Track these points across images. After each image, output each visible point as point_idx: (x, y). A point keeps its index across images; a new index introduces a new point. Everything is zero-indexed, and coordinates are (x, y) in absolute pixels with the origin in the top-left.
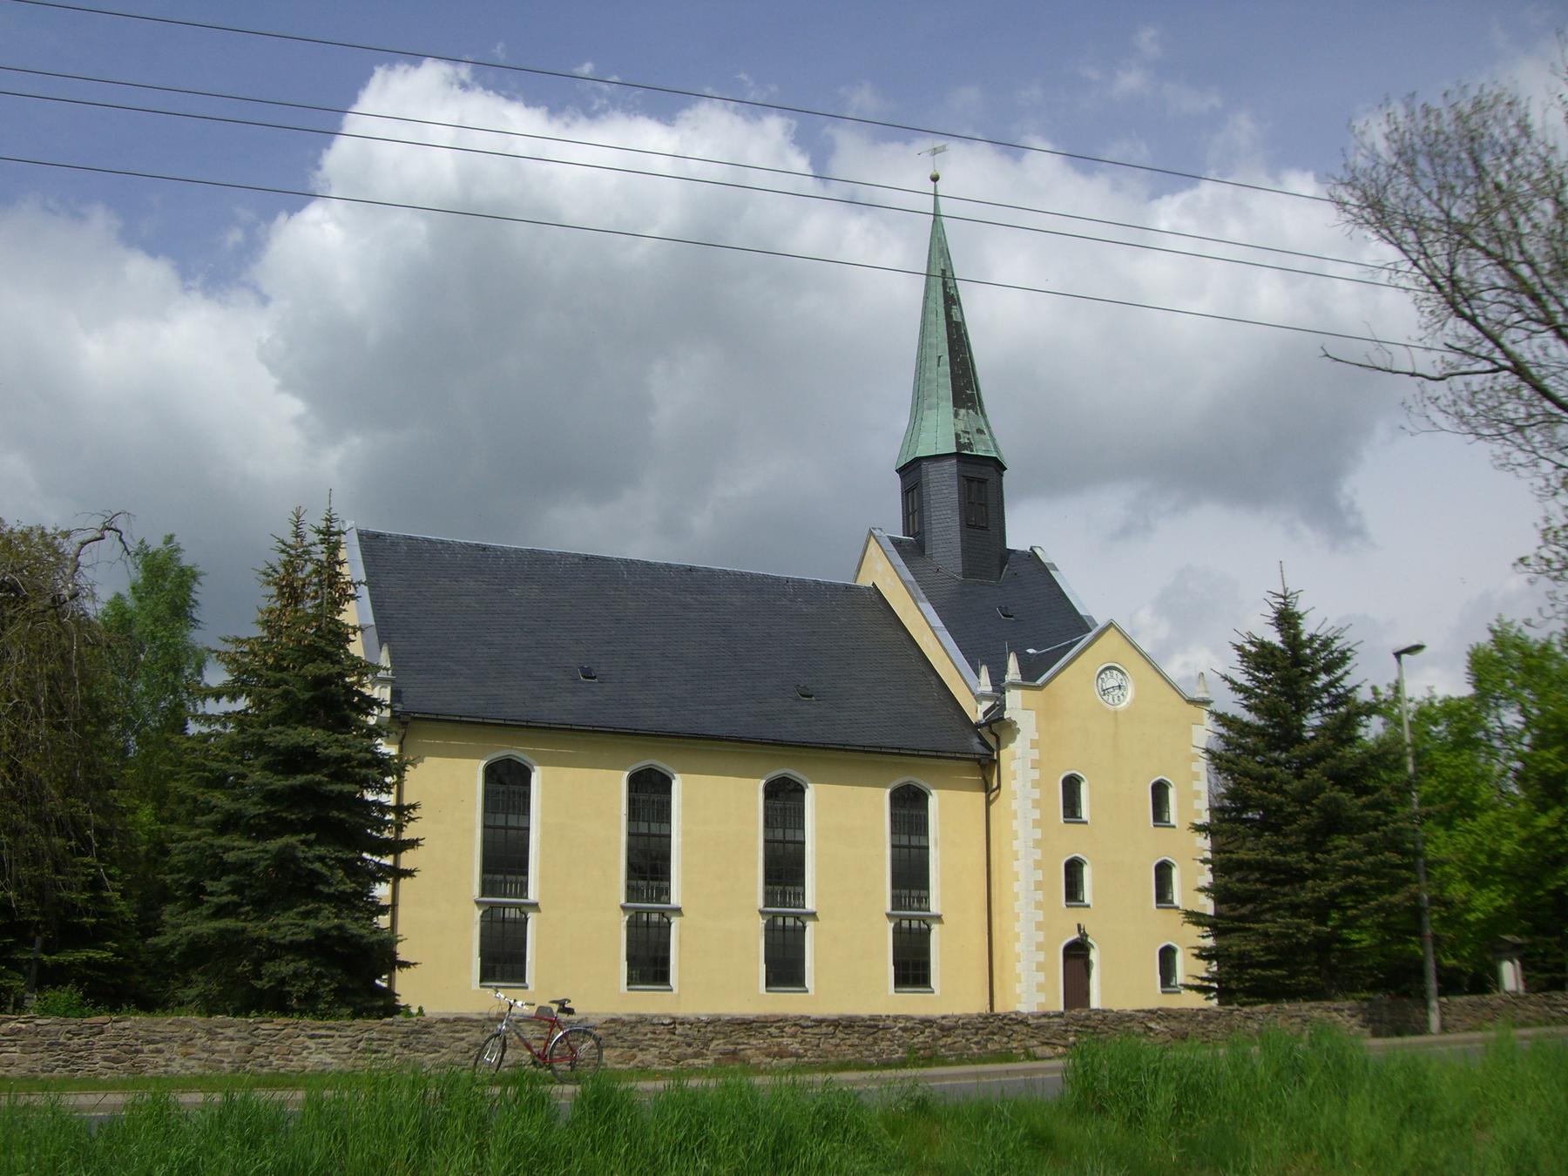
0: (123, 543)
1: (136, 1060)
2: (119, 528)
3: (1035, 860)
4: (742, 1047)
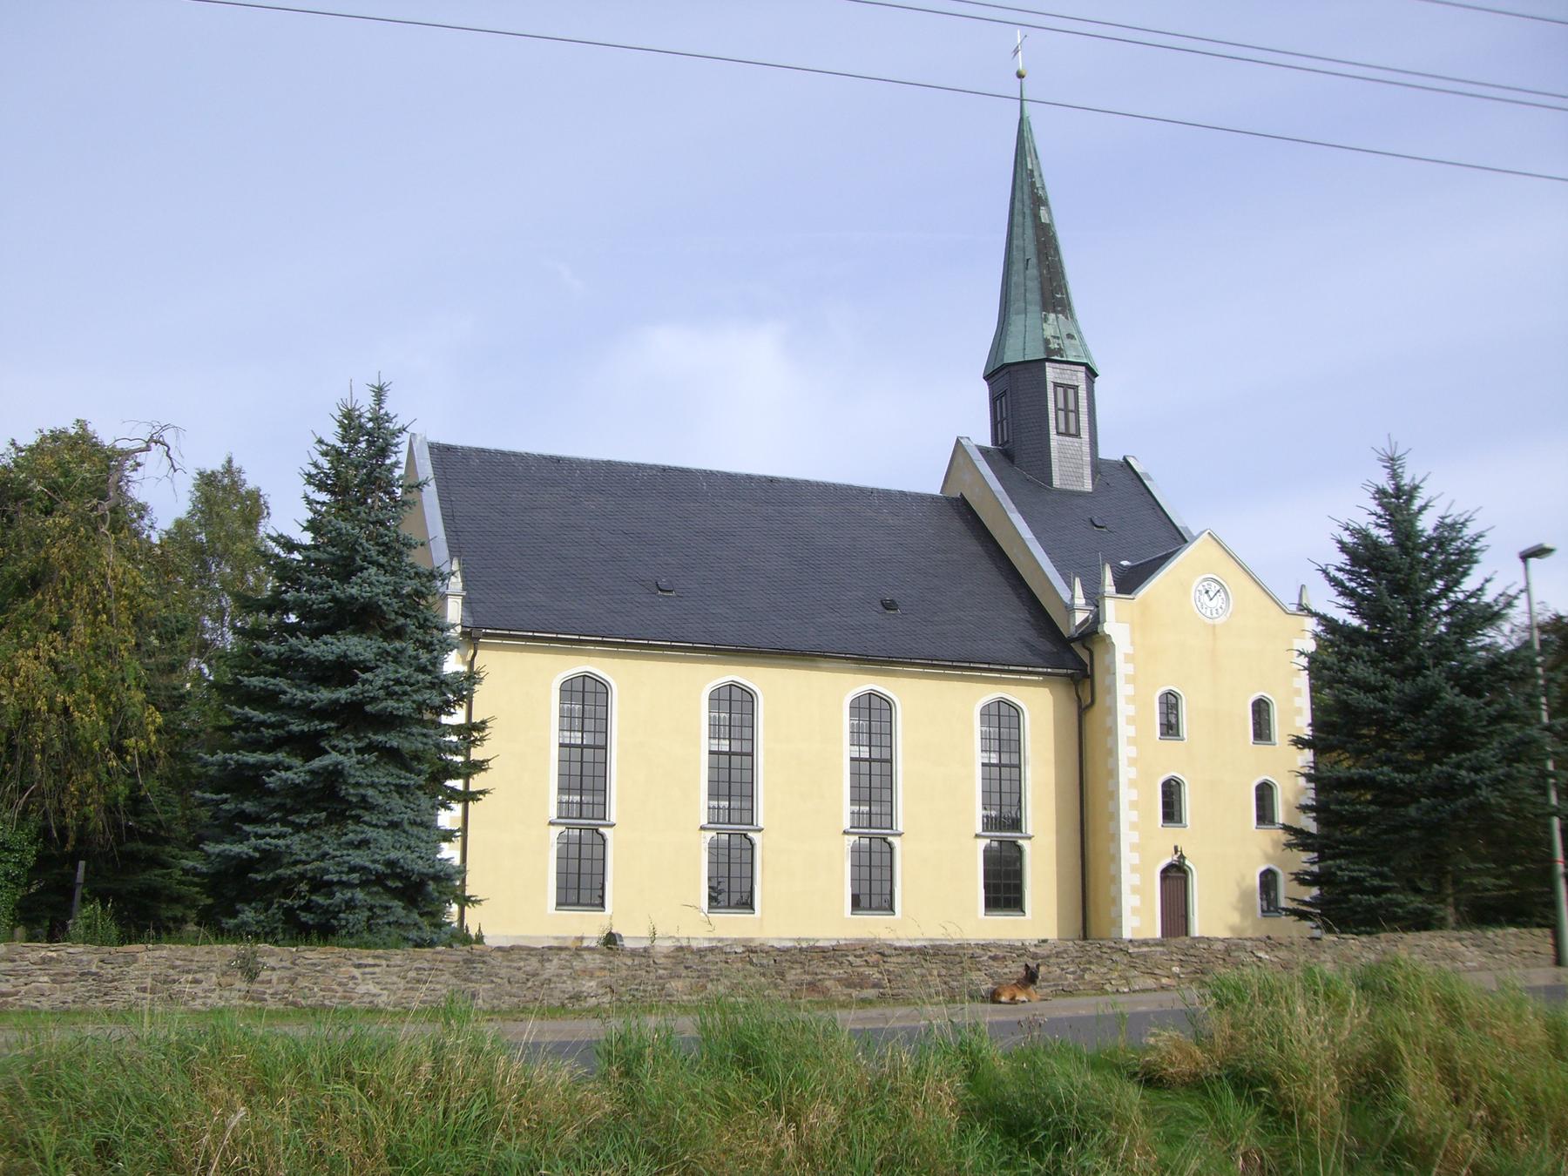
0: (171, 458)
2: (167, 442)
3: (1130, 779)
4: (819, 977)
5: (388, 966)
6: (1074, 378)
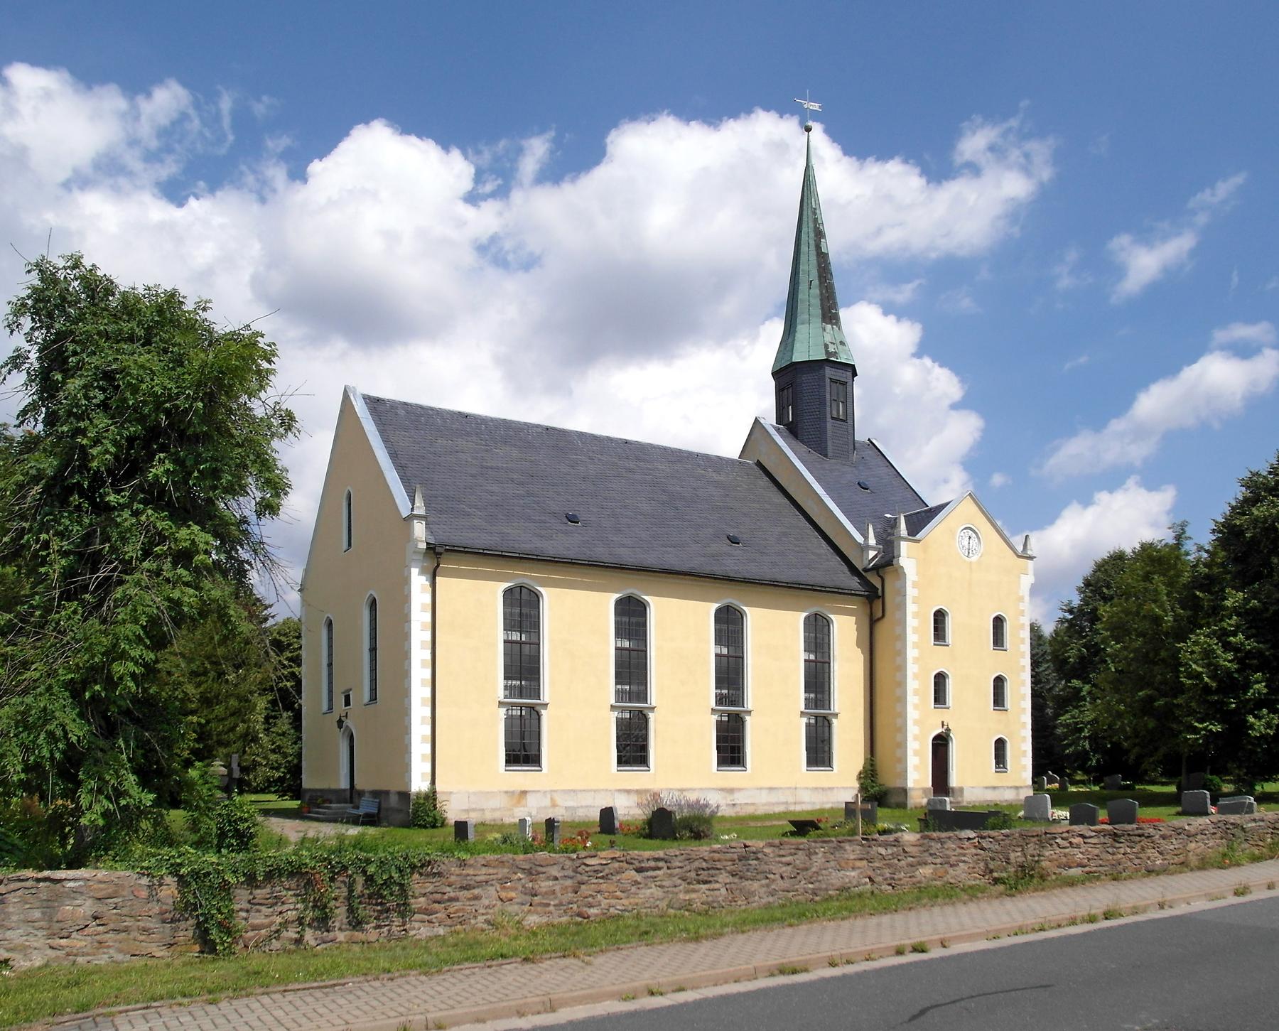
1: (451, 910)
5: (668, 868)
6: (844, 376)
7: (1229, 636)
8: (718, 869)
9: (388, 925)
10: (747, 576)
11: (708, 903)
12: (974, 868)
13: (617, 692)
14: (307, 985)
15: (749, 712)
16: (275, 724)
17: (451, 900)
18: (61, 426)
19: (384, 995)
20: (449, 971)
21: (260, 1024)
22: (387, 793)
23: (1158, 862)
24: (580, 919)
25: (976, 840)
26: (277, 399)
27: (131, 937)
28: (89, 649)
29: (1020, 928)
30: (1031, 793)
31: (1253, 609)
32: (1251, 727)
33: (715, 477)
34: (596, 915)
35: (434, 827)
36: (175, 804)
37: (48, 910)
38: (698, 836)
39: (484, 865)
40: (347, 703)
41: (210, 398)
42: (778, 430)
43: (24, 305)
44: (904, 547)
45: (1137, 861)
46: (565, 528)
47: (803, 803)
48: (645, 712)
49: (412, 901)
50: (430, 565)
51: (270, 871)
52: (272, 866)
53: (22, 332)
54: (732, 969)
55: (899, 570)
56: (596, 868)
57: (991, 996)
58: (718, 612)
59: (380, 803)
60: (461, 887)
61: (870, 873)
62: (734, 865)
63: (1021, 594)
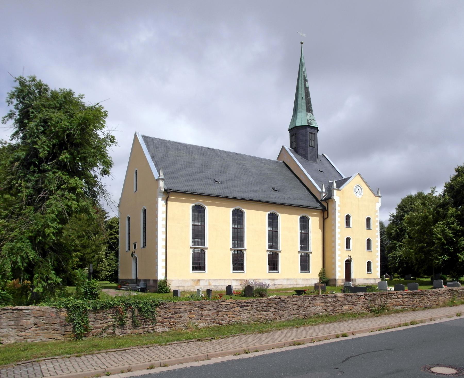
1: (171, 322)
5: (252, 306)
7: (450, 225)
8: (270, 306)
9: (147, 327)
10: (279, 202)
11: (266, 319)
12: (363, 306)
13: (233, 244)
14: (115, 350)
15: (280, 251)
16: (109, 256)
17: (171, 318)
18: (27, 140)
19: (144, 353)
20: (169, 344)
21: (96, 365)
22: (149, 280)
23: (428, 304)
24: (218, 325)
25: (364, 296)
26: (108, 132)
27: (49, 331)
28: (36, 224)
29: (381, 328)
30: (380, 281)
31: (459, 215)
32: (460, 258)
33: (268, 167)
34: (225, 324)
35: (166, 292)
36: (70, 284)
37: (17, 321)
38: (262, 296)
39: (183, 305)
40: (135, 247)
41: (83, 130)
42: (290, 150)
43: (14, 95)
44: (335, 192)
45: (421, 304)
46: (214, 184)
47: (300, 284)
48: (243, 251)
49: (156, 318)
50: (165, 197)
51: (103, 306)
52: (103, 304)
53: (13, 104)
54: (276, 343)
55: (334, 201)
56: (225, 306)
57: (372, 353)
58: (269, 215)
59: (146, 284)
60: (174, 313)
61: (325, 308)
62: (276, 305)
63: (376, 210)
